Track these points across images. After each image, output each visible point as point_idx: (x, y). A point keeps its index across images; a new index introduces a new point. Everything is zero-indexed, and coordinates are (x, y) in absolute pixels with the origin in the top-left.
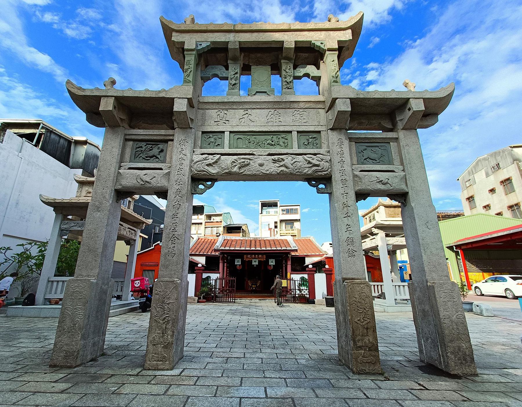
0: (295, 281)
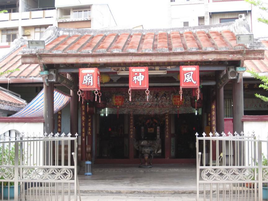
0: (260, 143)
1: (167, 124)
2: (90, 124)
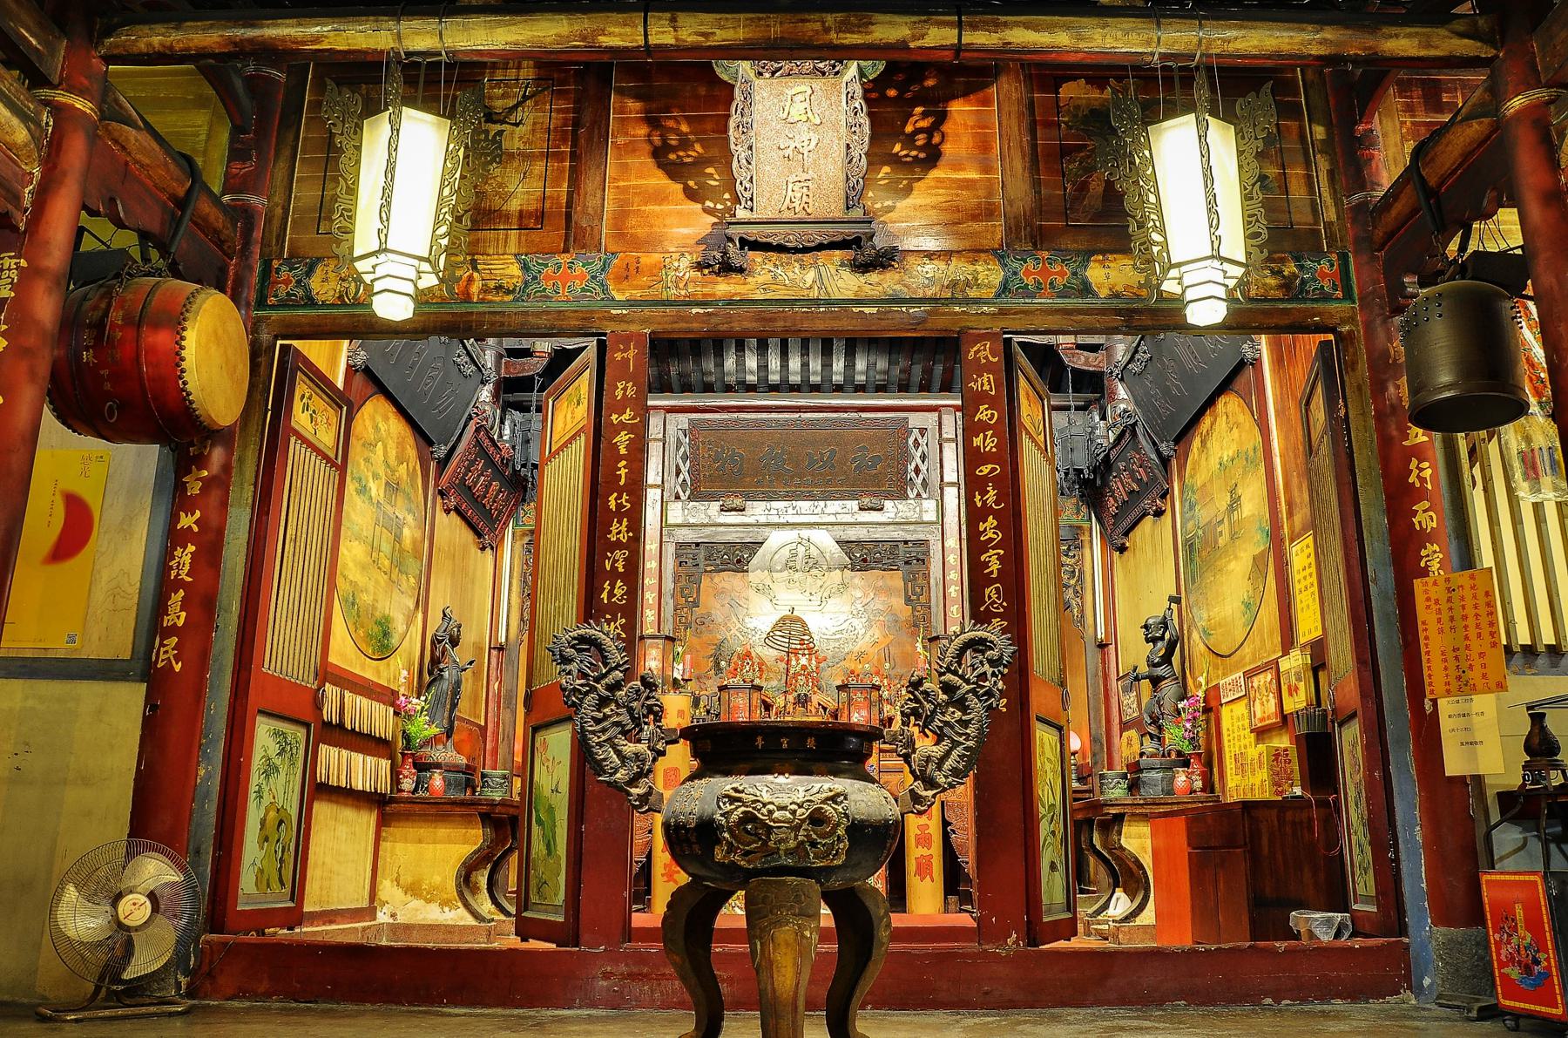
1: (995, 566)
2: (187, 559)
